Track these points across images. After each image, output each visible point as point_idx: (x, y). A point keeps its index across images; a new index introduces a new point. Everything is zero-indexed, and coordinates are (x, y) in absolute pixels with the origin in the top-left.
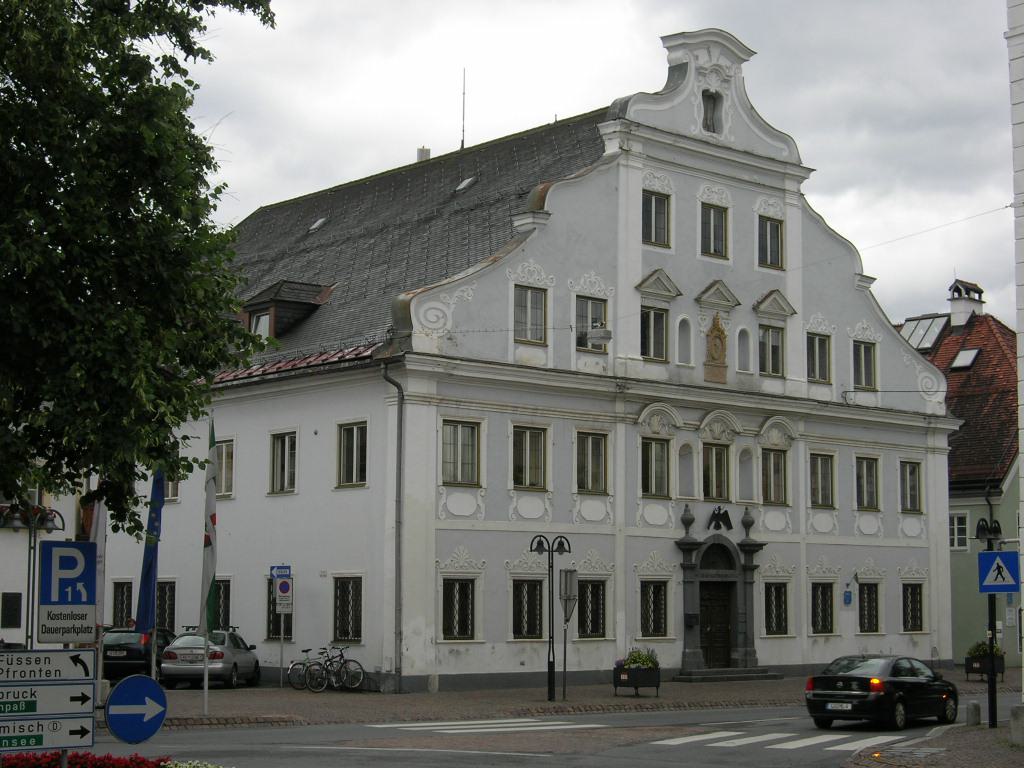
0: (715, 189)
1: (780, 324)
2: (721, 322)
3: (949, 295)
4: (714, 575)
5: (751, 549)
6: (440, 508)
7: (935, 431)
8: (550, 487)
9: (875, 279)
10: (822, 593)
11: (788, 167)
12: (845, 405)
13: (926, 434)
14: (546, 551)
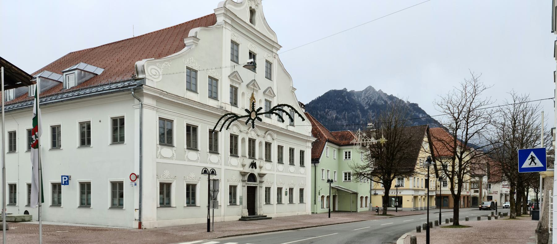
1: (270, 100)
2: (254, 95)
4: (252, 184)
5: (262, 175)
6: (158, 154)
7: (309, 141)
10: (280, 190)
11: (275, 43)
14: (207, 173)
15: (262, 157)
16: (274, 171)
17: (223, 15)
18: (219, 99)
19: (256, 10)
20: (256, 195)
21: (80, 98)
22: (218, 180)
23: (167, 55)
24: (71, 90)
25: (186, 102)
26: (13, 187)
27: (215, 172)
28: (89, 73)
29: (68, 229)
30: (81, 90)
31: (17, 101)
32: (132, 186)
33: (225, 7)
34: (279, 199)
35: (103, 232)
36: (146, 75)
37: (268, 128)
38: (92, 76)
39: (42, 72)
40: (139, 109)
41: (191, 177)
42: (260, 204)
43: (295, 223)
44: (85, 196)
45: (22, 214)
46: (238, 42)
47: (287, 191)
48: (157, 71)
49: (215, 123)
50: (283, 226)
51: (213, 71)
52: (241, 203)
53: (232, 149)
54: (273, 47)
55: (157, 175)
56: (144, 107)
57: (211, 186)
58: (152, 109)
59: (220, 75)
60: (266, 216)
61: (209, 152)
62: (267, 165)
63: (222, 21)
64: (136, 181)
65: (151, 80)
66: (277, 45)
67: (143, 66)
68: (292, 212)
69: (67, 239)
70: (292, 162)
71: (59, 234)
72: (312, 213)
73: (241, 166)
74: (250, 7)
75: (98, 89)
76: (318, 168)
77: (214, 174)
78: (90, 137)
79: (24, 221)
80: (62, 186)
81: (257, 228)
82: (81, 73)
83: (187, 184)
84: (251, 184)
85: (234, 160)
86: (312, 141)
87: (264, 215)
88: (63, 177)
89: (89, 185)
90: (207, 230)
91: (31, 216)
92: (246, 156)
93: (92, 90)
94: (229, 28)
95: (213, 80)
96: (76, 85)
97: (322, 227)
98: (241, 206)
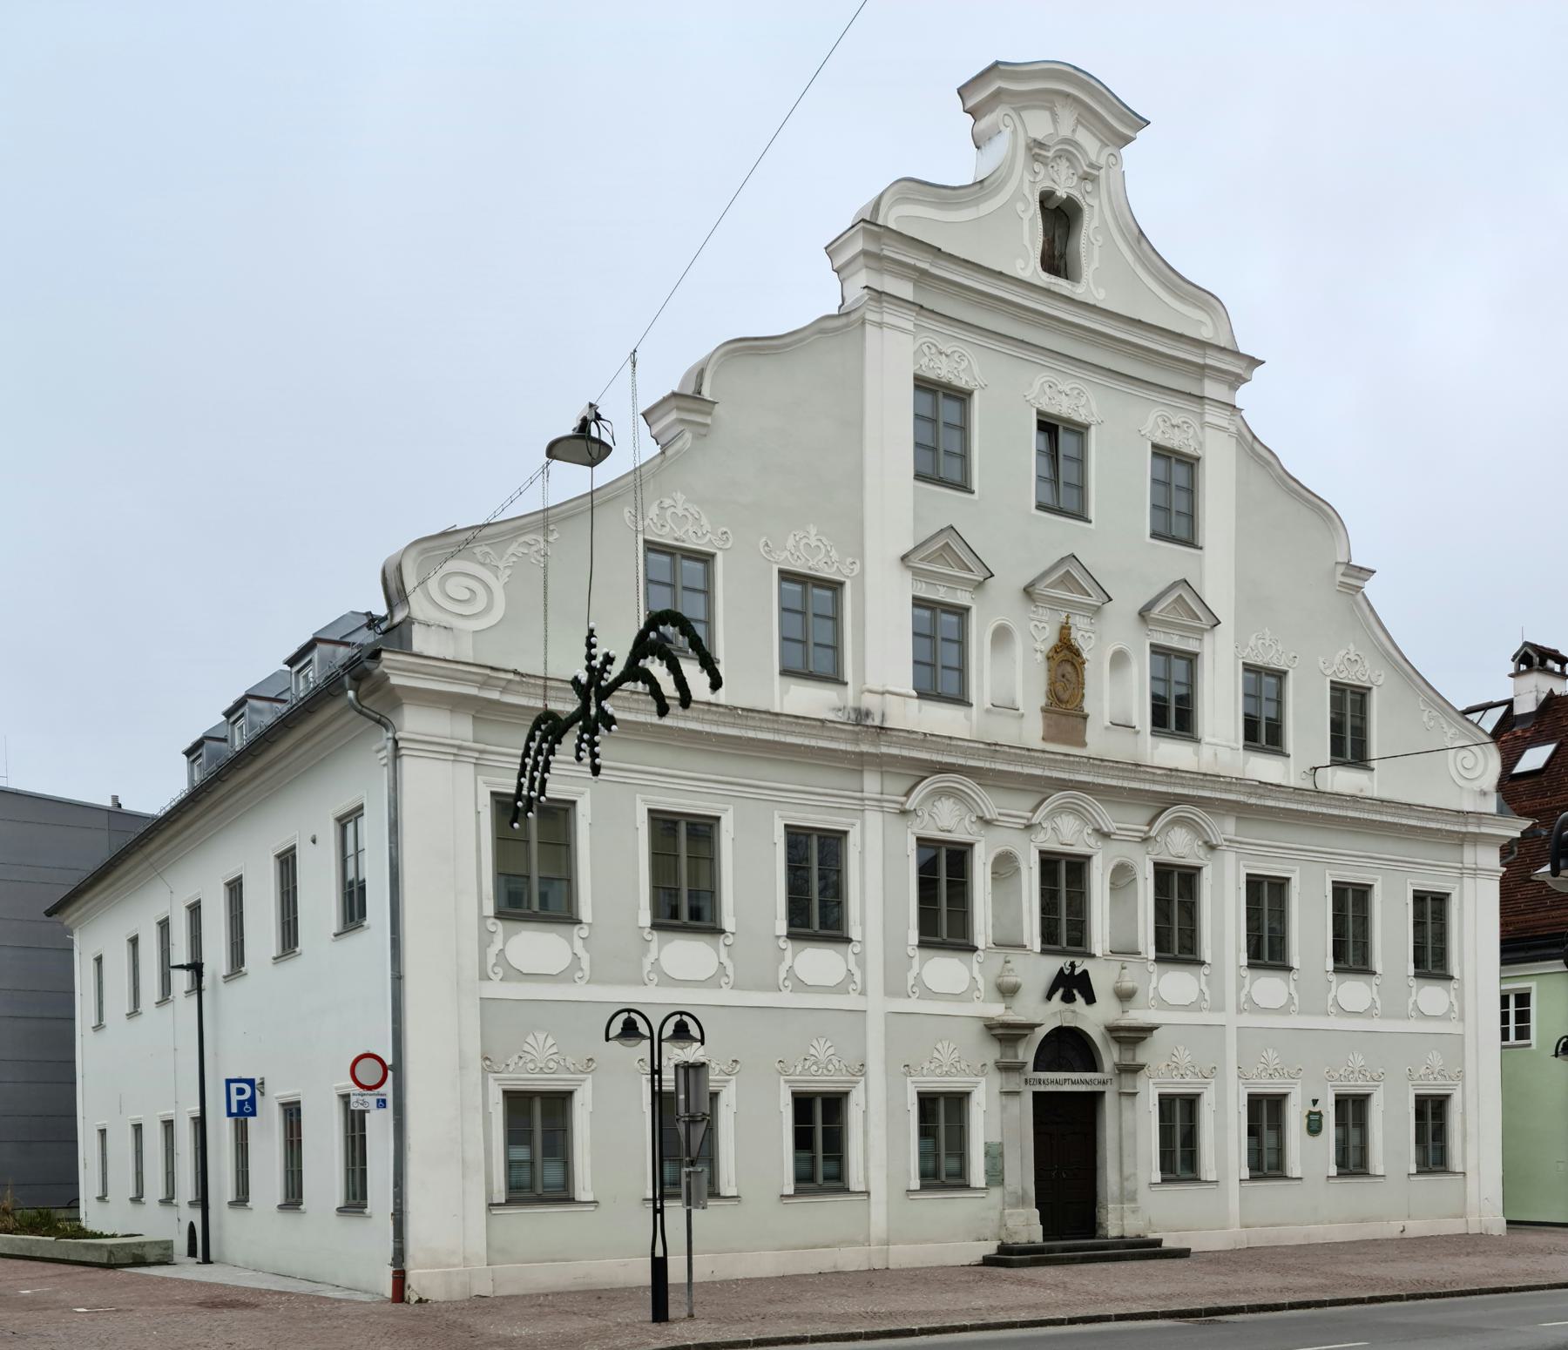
1: (1190, 645)
3: (1511, 668)
6: (491, 960)
7: (1477, 839)
8: (728, 923)
11: (1209, 352)
13: (1462, 845)
16: (1219, 1007)
17: (861, 260)
26: (138, 1128)
42: (1122, 1178)
47: (1319, 1113)
52: (995, 1176)
53: (1260, 938)
54: (1202, 370)
56: (403, 752)
58: (452, 758)
59: (850, 560)
60: (1158, 1243)
61: (1415, 976)
64: (381, 1090)
72: (1509, 1222)
73: (996, 995)
74: (1046, 198)
85: (945, 970)
87: (1152, 1236)
88: (234, 1087)
92: (1026, 942)
95: (810, 585)
98: (996, 1193)
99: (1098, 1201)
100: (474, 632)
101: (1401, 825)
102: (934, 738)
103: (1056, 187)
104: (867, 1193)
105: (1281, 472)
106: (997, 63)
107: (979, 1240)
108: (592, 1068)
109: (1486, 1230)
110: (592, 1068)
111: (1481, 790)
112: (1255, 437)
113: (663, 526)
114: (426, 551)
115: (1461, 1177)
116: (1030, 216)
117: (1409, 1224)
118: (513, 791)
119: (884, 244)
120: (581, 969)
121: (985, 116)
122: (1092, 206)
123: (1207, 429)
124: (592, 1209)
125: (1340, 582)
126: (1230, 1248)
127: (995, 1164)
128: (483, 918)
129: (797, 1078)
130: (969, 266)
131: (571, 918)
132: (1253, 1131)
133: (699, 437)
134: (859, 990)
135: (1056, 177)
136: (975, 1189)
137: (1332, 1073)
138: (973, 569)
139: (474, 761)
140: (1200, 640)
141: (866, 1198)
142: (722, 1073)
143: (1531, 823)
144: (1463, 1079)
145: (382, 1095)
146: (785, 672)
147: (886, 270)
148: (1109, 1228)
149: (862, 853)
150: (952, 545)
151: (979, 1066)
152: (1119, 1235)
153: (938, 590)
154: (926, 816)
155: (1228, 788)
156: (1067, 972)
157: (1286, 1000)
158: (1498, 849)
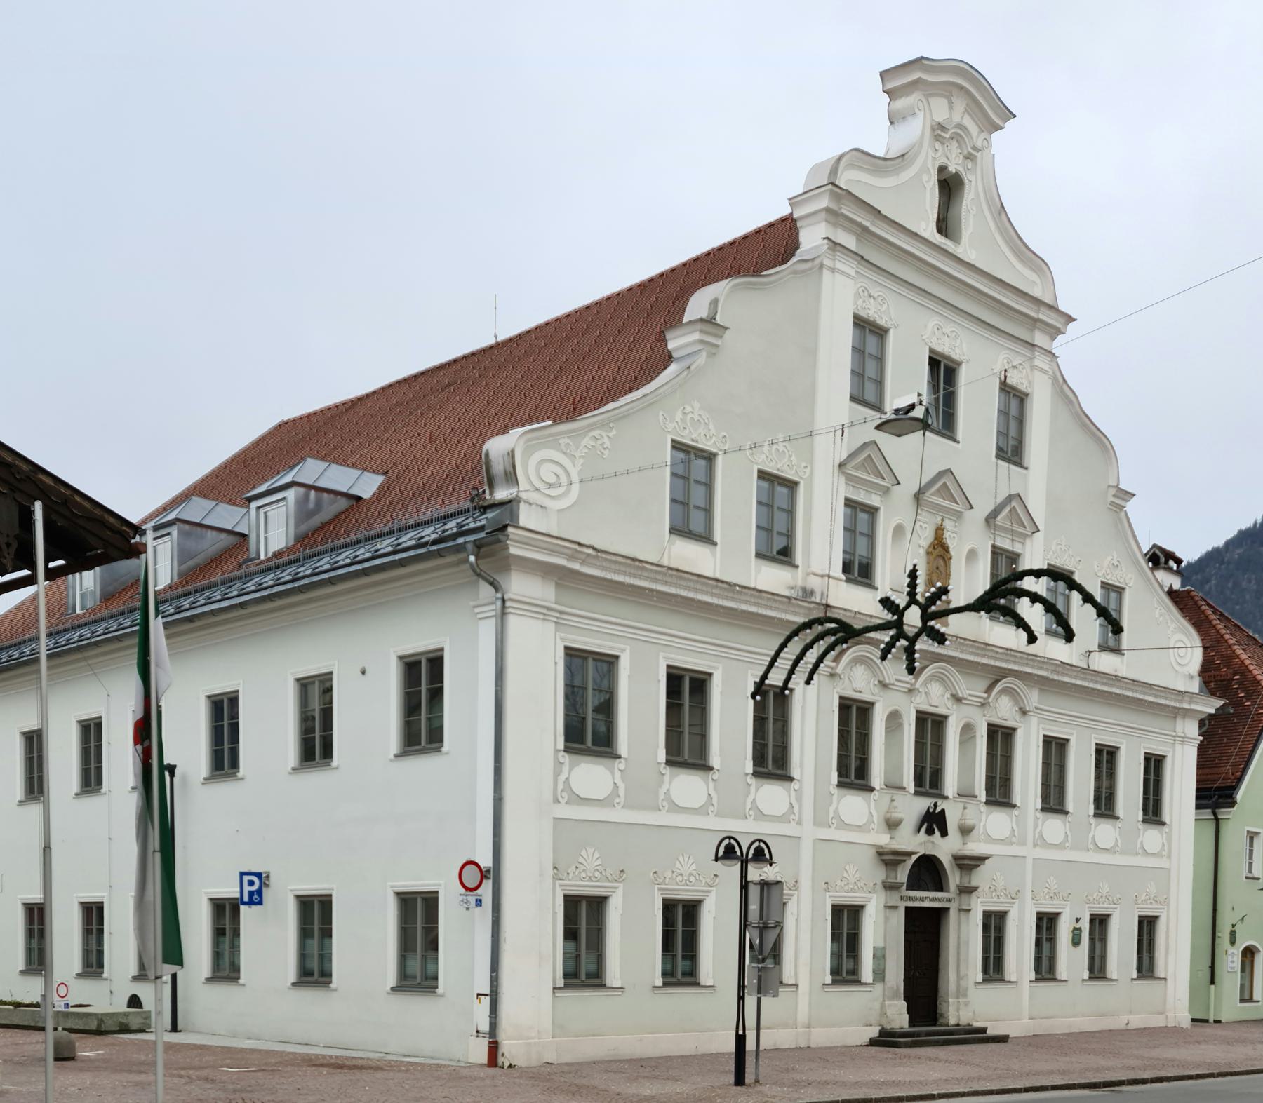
0: (947, 330)
2: (947, 535)
4: (927, 899)
6: (560, 787)
7: (1186, 713)
9: (1134, 495)
10: (1047, 924)
11: (1043, 309)
12: (1086, 672)
13: (1175, 718)
14: (736, 858)
15: (974, 791)
16: (1023, 843)
17: (823, 215)
18: (799, 557)
19: (966, 177)
20: (942, 941)
21: (301, 590)
22: (778, 882)
23: (603, 402)
24: (271, 564)
25: (666, 583)
27: (766, 852)
28: (332, 496)
29: (256, 1062)
30: (304, 559)
31: (105, 613)
32: (468, 909)
33: (833, 184)
34: (1045, 963)
35: (365, 1076)
36: (521, 489)
37: (1003, 665)
38: (343, 504)
39: (183, 502)
40: (494, 620)
41: (681, 875)
42: (959, 978)
43: (1103, 1062)
44: (313, 945)
45: (121, 1006)
46: (882, 322)
48: (562, 466)
49: (767, 655)
50: (1052, 1072)
51: (777, 450)
52: (879, 975)
54: (1034, 323)
55: (555, 868)
57: (754, 907)
58: (541, 617)
59: (804, 464)
60: (984, 1030)
62: (996, 822)
63: (820, 242)
64: (478, 891)
65: (537, 505)
66: (1054, 315)
67: (512, 454)
68: (1103, 1015)
69: (249, 1095)
70: (1105, 804)
71: (224, 1078)
72: (1193, 1020)
73: (884, 826)
74: (942, 169)
75: (358, 553)
76: (1226, 830)
77: (765, 861)
78: (331, 730)
79: (125, 1029)
80: (243, 908)
81: (937, 1075)
82: (307, 497)
83: (664, 900)
84: (921, 900)
85: (853, 805)
86: (1203, 712)
88: (246, 878)
89: (325, 903)
90: (732, 1080)
91: (147, 1016)
92: (905, 785)
93: (338, 559)
94: (847, 266)
96: (291, 542)
97: (1229, 1078)
98: (879, 987)
99: (939, 995)
100: (558, 510)
101: (1145, 701)
102: (861, 616)
103: (949, 163)
104: (796, 985)
105: (1079, 409)
106: (922, 58)
107: (867, 1026)
108: (623, 878)
109: (1179, 1024)
110: (623, 878)
111: (1190, 674)
112: (1064, 380)
113: (684, 428)
114: (528, 440)
115: (1163, 982)
116: (931, 186)
117: (1131, 1017)
118: (781, 684)
119: (843, 204)
120: (619, 796)
121: (901, 97)
122: (971, 181)
123: (1036, 371)
124: (620, 993)
125: (1112, 502)
126: (1023, 1035)
127: (879, 964)
128: (557, 751)
129: (846, 894)
130: (896, 226)
131: (612, 753)
132: (1038, 943)
133: (712, 355)
134: (622, 804)
135: (949, 154)
136: (866, 984)
137: (1089, 897)
138: (885, 478)
139: (555, 620)
140: (1023, 543)
141: (794, 989)
142: (707, 885)
143: (1222, 702)
144: (1168, 905)
145: (479, 896)
146: (759, 555)
147: (840, 225)
148: (950, 1017)
149: (803, 707)
150: (873, 457)
151: (872, 884)
152: (956, 1023)
153: (860, 492)
154: (846, 679)
155: (1041, 665)
156: (931, 810)
157: (1062, 838)
158: (1198, 722)
